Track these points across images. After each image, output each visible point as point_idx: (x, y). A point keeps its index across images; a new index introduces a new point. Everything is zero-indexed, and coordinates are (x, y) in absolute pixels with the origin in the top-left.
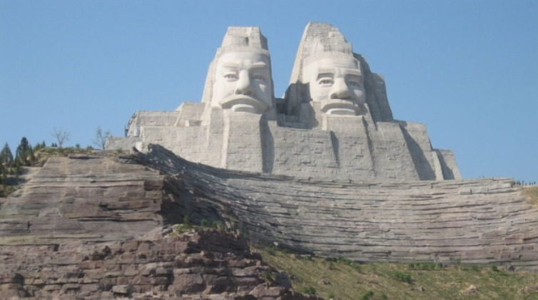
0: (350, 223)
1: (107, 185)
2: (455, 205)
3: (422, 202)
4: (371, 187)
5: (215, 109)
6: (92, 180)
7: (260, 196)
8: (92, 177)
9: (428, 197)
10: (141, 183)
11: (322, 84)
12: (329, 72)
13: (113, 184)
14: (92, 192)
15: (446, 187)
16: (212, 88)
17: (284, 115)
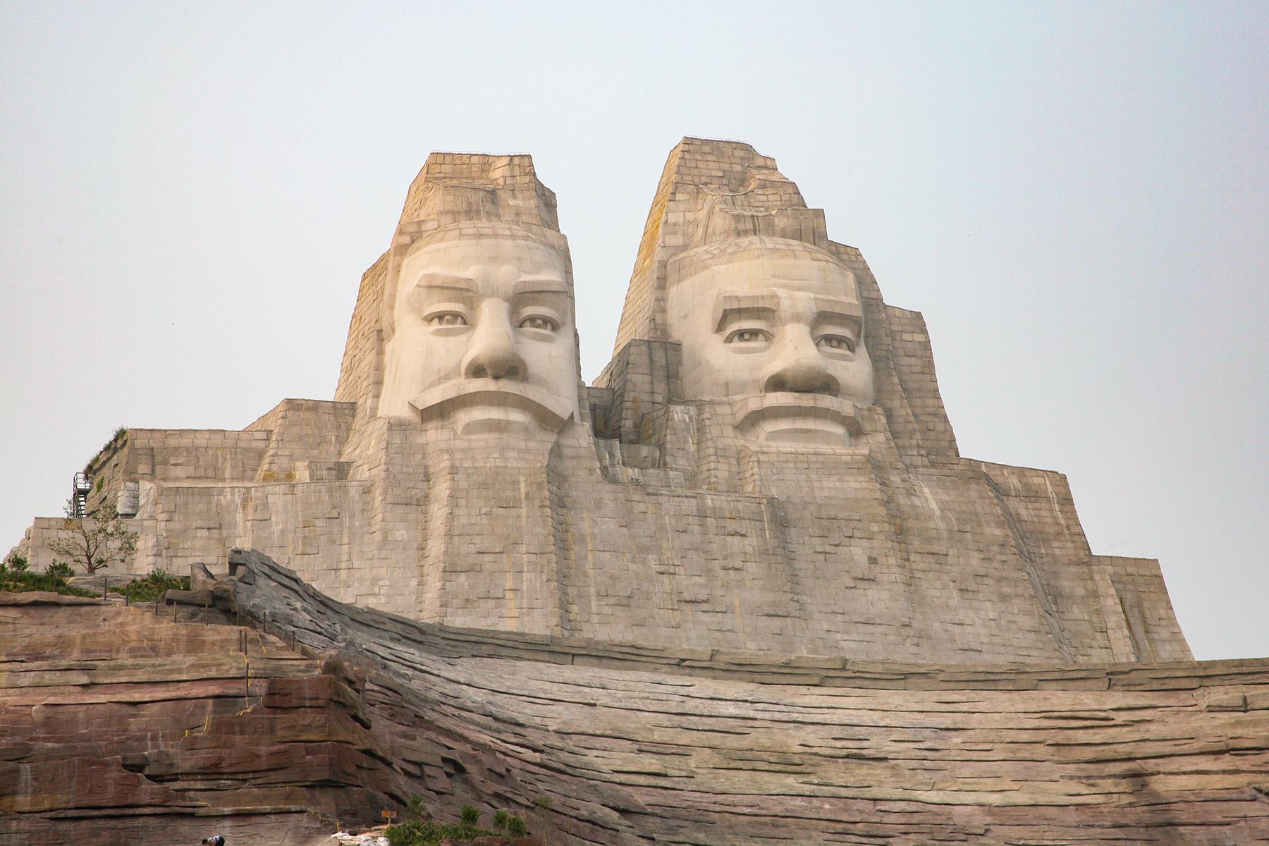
0: (860, 805)
1: (137, 697)
2: (1196, 746)
3: (1082, 736)
4: (913, 680)
5: (397, 426)
6: (84, 679)
7: (566, 717)
8: (85, 669)
9: (1104, 722)
10: (260, 688)
11: (737, 344)
12: (761, 304)
13: (160, 693)
14: (88, 722)
15: (1156, 685)
16: (380, 353)
17: (616, 443)
